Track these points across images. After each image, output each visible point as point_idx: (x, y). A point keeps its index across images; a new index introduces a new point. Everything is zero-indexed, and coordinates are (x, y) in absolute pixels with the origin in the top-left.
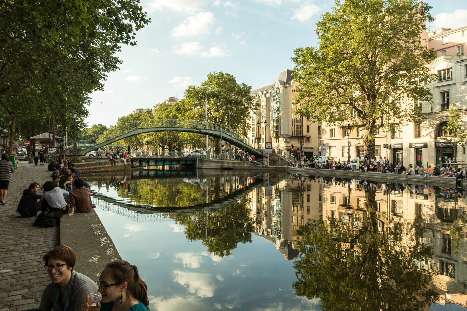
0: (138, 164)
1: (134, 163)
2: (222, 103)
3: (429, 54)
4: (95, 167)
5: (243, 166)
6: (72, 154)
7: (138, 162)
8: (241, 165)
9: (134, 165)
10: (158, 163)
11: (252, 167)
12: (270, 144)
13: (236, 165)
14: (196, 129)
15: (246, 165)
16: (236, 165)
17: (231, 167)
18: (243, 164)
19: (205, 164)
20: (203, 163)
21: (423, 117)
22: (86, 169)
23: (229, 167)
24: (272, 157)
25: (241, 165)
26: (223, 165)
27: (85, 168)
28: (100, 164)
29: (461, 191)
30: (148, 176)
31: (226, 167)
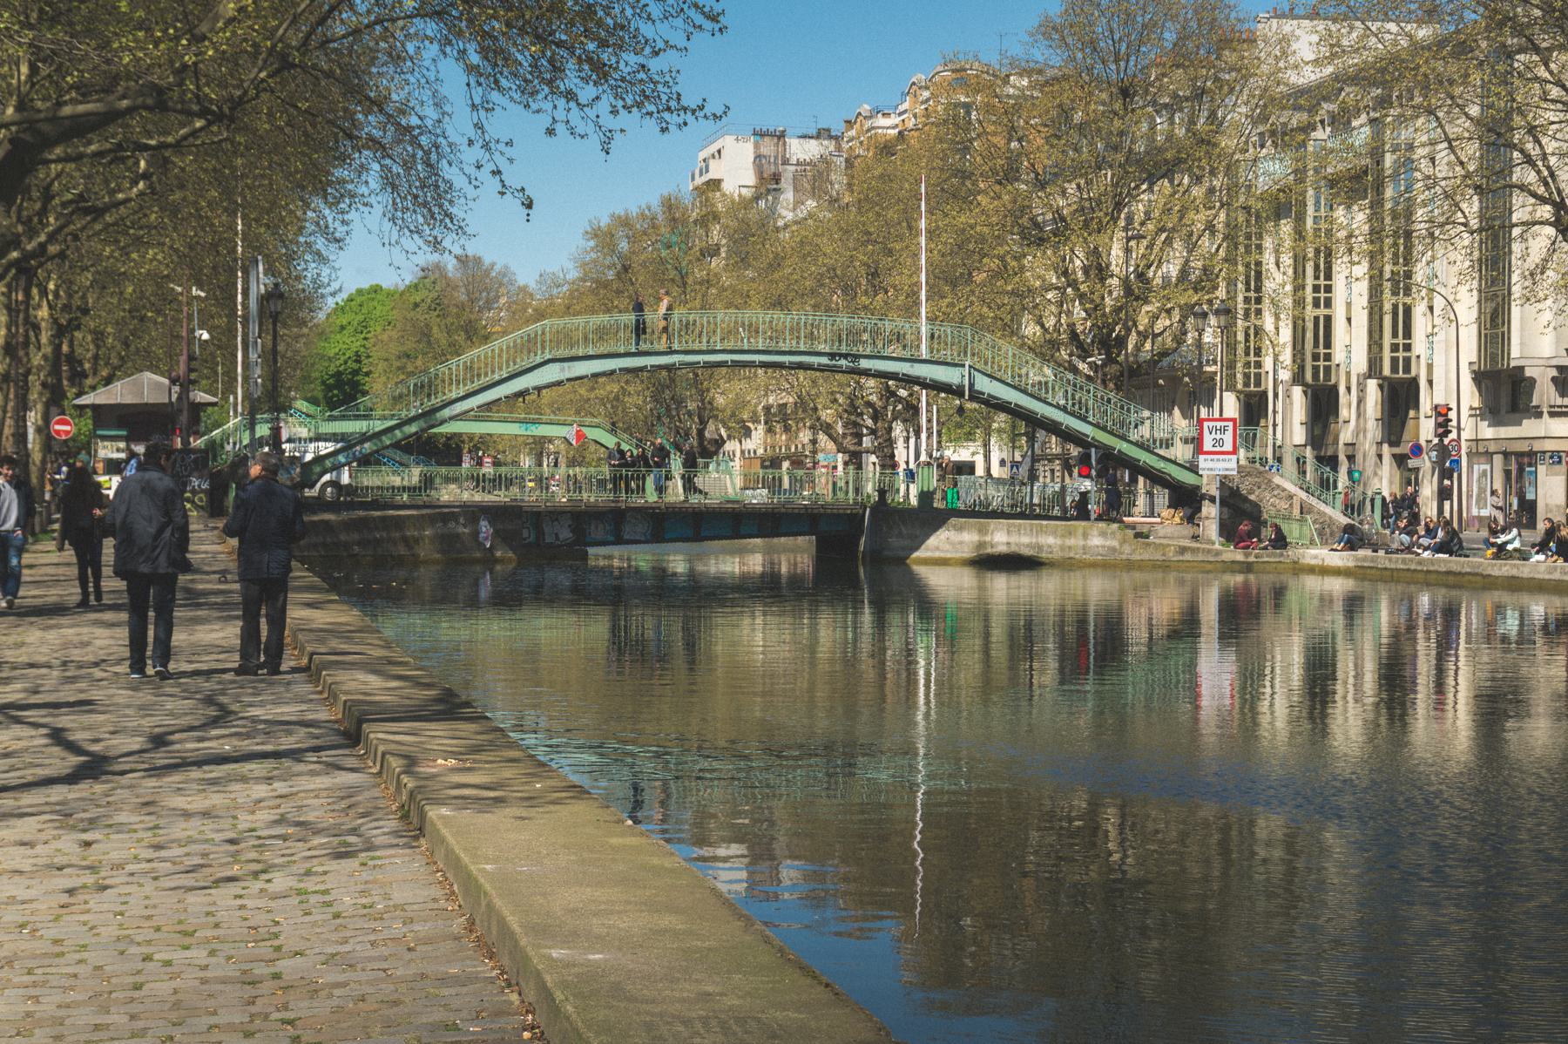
2: (226, 316)
5: (1081, 543)
9: (548, 540)
11: (1127, 549)
12: (1224, 430)
17: (1027, 552)
18: (1085, 536)
19: (900, 535)
21: (152, 174)
23: (1014, 549)
26: (988, 539)
29: (653, 1038)
30: (300, 439)
31: (1002, 549)
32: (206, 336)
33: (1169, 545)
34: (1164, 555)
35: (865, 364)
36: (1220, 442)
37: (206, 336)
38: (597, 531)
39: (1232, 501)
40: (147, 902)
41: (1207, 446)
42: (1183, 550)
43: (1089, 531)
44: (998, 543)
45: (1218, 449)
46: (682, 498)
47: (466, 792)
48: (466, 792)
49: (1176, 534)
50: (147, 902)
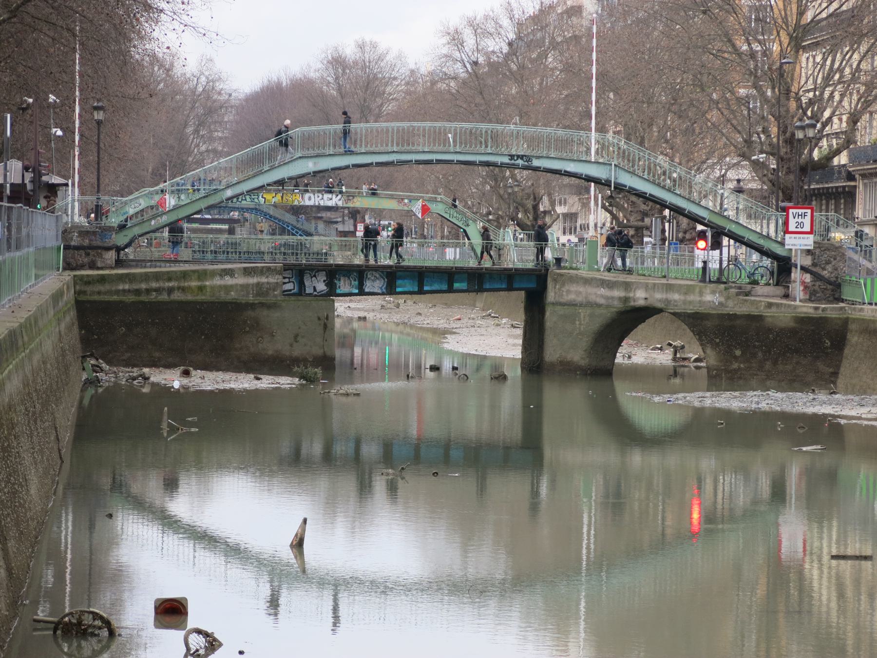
0: (321, 287)
1: (307, 283)
3: (454, 91)
4: (154, 285)
5: (698, 299)
6: (86, 242)
7: (322, 277)
8: (691, 298)
9: (309, 290)
10: (399, 282)
11: (730, 303)
13: (676, 296)
14: (512, 157)
15: (708, 298)
16: (676, 296)
17: (659, 305)
18: (701, 294)
20: (563, 285)
22: (124, 291)
24: (829, 268)
25: (691, 298)
26: (631, 295)
27: (121, 287)
28: (169, 276)
31: (641, 303)
32: (59, 133)
33: (761, 301)
34: (757, 308)
35: (536, 163)
36: (801, 224)
37: (59, 133)
38: (344, 286)
39: (814, 269)
40: (382, 619)
41: (792, 228)
42: (770, 305)
43: (704, 290)
44: (638, 298)
45: (799, 230)
46: (396, 261)
47: (871, 486)
48: (871, 486)
49: (771, 294)
50: (382, 619)
